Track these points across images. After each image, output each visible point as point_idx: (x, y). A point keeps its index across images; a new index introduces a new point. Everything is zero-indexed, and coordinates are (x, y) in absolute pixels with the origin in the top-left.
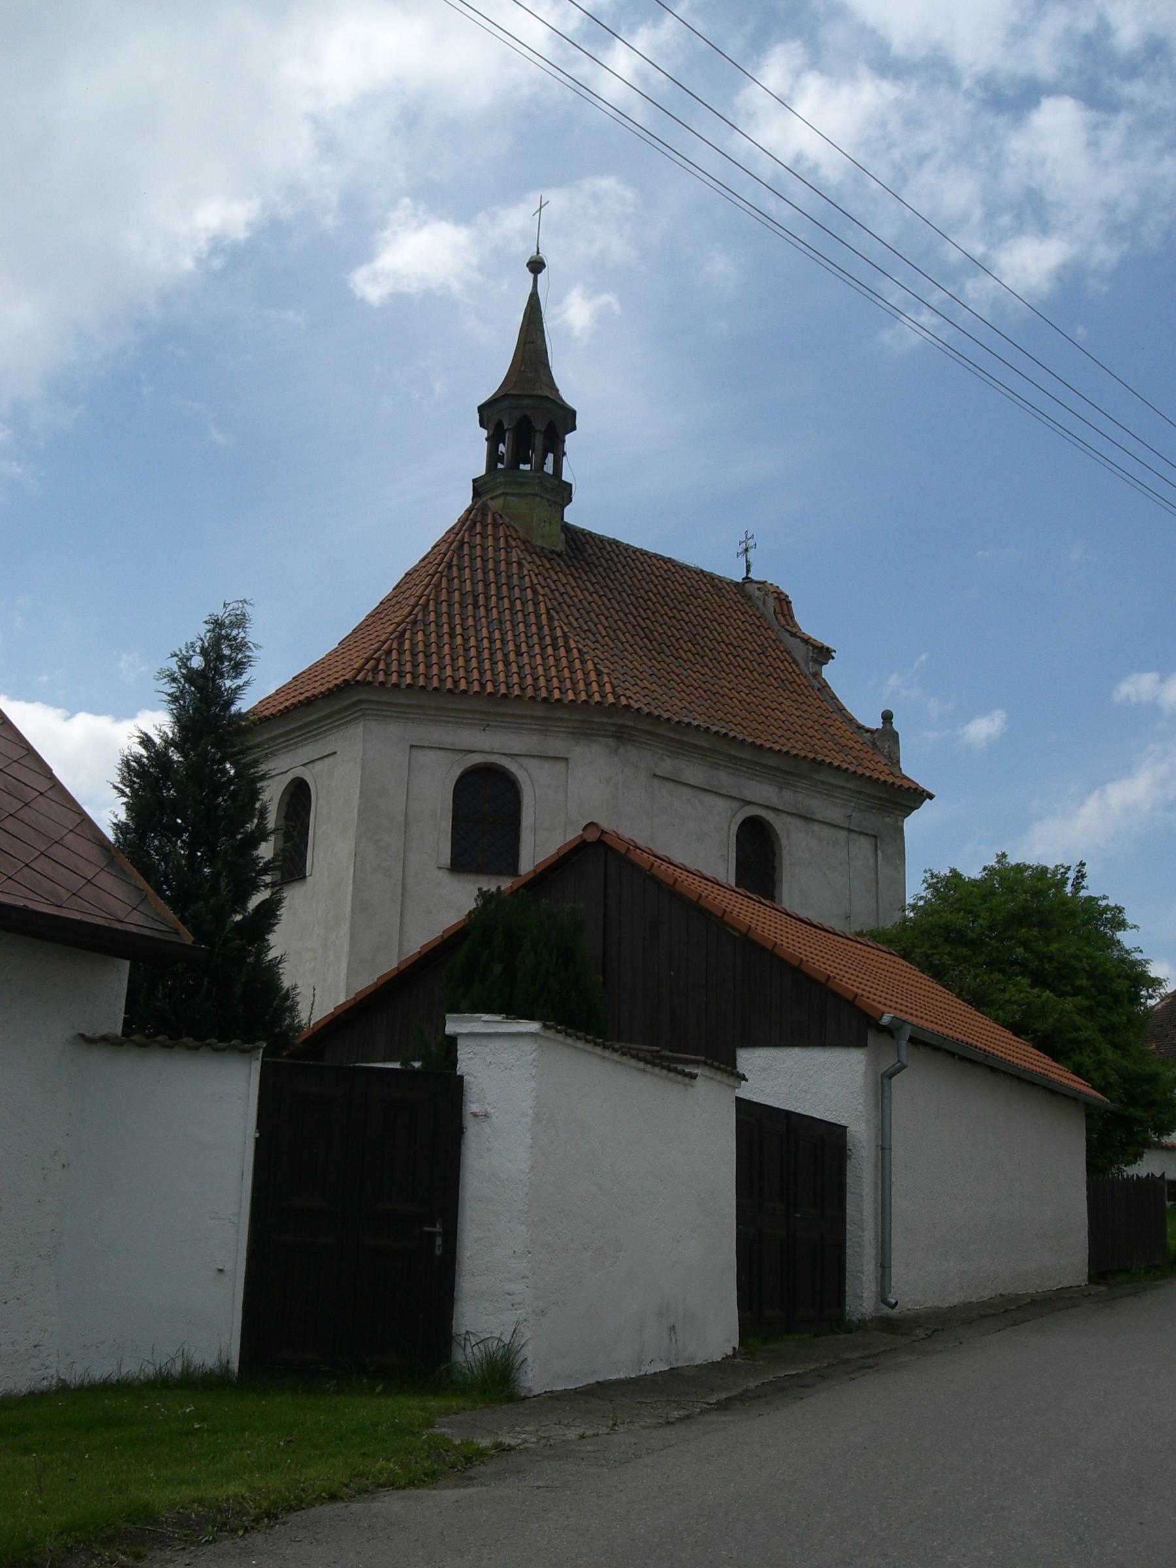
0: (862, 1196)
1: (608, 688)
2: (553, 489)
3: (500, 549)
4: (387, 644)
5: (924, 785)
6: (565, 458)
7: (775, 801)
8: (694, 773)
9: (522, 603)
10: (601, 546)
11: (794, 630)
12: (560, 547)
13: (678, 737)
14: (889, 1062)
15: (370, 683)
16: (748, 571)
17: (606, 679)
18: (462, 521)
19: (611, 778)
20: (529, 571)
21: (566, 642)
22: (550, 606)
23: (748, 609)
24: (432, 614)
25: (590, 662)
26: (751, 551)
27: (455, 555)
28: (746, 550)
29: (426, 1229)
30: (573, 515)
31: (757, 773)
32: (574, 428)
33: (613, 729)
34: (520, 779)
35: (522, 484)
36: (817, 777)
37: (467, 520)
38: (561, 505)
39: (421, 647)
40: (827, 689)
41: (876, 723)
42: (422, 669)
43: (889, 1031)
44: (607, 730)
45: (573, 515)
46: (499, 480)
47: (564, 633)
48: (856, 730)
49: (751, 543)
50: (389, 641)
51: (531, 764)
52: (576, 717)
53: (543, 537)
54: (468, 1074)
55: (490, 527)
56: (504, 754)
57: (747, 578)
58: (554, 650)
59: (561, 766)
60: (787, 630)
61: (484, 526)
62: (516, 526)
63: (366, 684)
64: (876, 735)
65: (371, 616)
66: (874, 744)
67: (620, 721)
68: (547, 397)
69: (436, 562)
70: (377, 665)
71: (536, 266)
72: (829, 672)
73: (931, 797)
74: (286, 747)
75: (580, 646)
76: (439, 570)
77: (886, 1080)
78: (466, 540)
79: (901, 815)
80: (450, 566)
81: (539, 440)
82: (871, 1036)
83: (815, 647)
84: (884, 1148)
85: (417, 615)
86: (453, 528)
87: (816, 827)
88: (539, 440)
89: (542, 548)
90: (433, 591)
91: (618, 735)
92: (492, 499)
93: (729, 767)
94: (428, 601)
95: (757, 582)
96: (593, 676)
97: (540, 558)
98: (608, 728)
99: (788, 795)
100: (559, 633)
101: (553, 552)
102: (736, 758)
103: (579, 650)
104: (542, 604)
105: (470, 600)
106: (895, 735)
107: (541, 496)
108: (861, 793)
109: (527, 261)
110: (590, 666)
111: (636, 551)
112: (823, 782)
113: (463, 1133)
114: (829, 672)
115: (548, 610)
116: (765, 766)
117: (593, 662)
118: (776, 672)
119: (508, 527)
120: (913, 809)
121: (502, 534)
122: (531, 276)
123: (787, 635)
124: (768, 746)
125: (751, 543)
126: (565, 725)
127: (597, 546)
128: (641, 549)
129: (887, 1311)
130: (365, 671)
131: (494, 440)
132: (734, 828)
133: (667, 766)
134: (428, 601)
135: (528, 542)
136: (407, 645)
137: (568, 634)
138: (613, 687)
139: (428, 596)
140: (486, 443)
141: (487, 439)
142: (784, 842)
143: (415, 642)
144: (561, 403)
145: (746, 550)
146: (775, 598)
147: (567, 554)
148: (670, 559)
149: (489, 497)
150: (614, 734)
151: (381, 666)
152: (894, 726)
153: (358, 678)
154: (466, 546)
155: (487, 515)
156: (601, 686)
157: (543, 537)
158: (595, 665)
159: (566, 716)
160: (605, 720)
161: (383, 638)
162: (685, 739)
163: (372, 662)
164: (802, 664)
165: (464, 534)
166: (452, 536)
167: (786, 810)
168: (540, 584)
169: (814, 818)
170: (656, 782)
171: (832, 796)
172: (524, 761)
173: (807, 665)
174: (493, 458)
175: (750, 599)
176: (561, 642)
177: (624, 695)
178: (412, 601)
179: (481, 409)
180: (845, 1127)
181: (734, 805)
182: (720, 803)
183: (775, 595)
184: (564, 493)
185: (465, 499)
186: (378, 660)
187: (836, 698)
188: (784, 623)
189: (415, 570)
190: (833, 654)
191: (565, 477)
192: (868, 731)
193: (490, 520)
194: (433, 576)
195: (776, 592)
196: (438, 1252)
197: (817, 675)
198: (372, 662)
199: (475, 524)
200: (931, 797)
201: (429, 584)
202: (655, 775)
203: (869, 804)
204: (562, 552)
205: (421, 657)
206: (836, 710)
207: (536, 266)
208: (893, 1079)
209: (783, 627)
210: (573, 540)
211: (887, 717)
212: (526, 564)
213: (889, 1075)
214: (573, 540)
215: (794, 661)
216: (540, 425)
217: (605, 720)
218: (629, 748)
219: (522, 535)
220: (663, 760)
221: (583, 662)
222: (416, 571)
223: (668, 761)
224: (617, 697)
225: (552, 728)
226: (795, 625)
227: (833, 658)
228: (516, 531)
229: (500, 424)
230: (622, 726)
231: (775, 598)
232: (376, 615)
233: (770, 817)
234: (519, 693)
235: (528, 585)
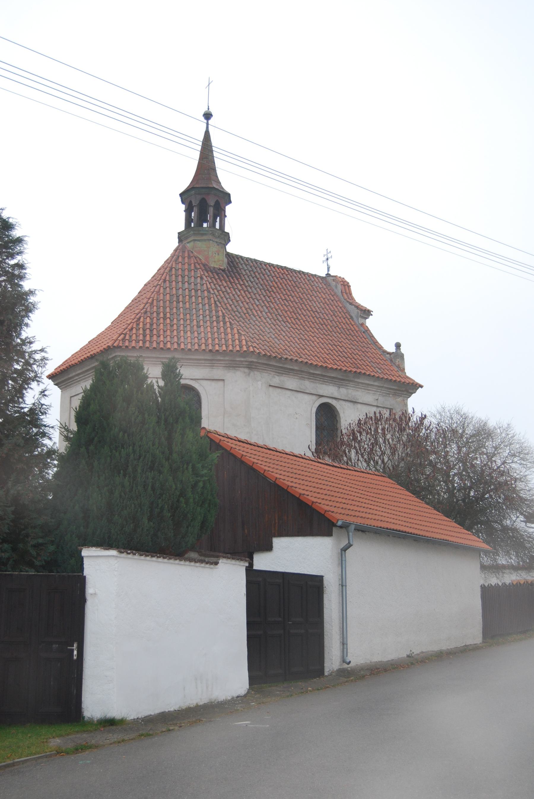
0: (331, 610)
1: (244, 342)
2: (219, 236)
3: (191, 270)
4: (130, 325)
5: (418, 380)
6: (226, 219)
7: (336, 395)
8: (291, 382)
9: (202, 298)
10: (247, 263)
11: (351, 301)
12: (224, 266)
13: (281, 365)
14: (344, 543)
15: (121, 347)
16: (328, 270)
17: (243, 338)
18: (172, 256)
19: (247, 389)
20: (206, 281)
21: (224, 319)
22: (216, 299)
23: (328, 291)
24: (155, 307)
25: (235, 329)
26: (329, 260)
27: (168, 275)
28: (327, 259)
29: (69, 648)
30: (231, 248)
31: (326, 381)
32: (179, 233)
33: (247, 363)
34: (200, 391)
35: (203, 235)
36: (356, 380)
37: (174, 255)
38: (224, 244)
39: (148, 326)
40: (368, 332)
41: (391, 348)
42: (148, 338)
43: (345, 527)
44: (243, 364)
45: (231, 248)
46: (191, 233)
47: (223, 314)
48: (382, 353)
49: (329, 255)
50: (132, 324)
51: (205, 383)
52: (227, 358)
53: (215, 262)
54: (88, 575)
55: (186, 258)
56: (191, 379)
57: (328, 275)
58: (217, 323)
59: (221, 383)
60: (348, 301)
61: (184, 258)
62: (200, 257)
63: (119, 347)
64: (392, 356)
65: (127, 308)
66: (391, 361)
67: (250, 360)
68: (214, 188)
69: (158, 279)
70: (125, 337)
71: (208, 116)
72: (370, 323)
73: (421, 387)
74: (83, 379)
75: (231, 320)
76: (159, 284)
77: (343, 552)
78: (173, 266)
79: (405, 397)
80: (165, 281)
81: (211, 210)
82: (334, 529)
83: (361, 310)
84: (343, 585)
85: (147, 309)
86: (168, 260)
87: (359, 406)
88: (211, 210)
89: (214, 268)
90: (156, 295)
91: (250, 366)
92: (188, 243)
93: (310, 379)
94: (153, 300)
95: (333, 276)
96: (237, 336)
97: (212, 273)
98: (244, 363)
99: (343, 391)
100: (220, 313)
101: (220, 269)
102: (314, 374)
103: (230, 322)
104: (212, 299)
105: (175, 299)
106: (402, 356)
107: (212, 240)
108: (382, 387)
109: (203, 114)
110: (236, 331)
111: (266, 264)
112: (362, 383)
113: (86, 602)
114: (370, 323)
115: (215, 302)
116: (330, 377)
117: (237, 329)
118: (341, 325)
119: (196, 258)
120: (412, 393)
121: (192, 262)
122: (206, 121)
123: (348, 304)
124: (330, 367)
125: (329, 255)
126: (222, 363)
127: (245, 264)
128: (270, 263)
129: (345, 666)
130: (118, 341)
131: (188, 211)
132: (314, 410)
133: (276, 380)
134: (153, 300)
135: (207, 265)
136: (141, 325)
137: (225, 314)
138: (246, 342)
139: (153, 298)
140: (184, 213)
141: (185, 211)
142: (341, 415)
143: (145, 323)
144: (221, 190)
145: (327, 259)
146: (341, 285)
147: (228, 270)
148: (285, 267)
149: (186, 242)
150: (248, 366)
151: (127, 337)
152: (401, 350)
153: (114, 345)
154: (173, 269)
155: (185, 252)
156: (240, 341)
157: (215, 262)
158: (238, 330)
159: (222, 358)
160: (242, 359)
161: (128, 322)
162: (285, 366)
163: (122, 336)
164: (355, 319)
165: (173, 263)
166: (167, 264)
167: (342, 398)
168: (211, 288)
169: (357, 401)
170: (271, 389)
171: (368, 390)
172: (202, 382)
173: (358, 319)
174: (188, 220)
175: (329, 285)
176: (221, 319)
177: (252, 346)
178: (145, 301)
179: (181, 195)
180: (322, 577)
181: (314, 397)
182: (306, 397)
183: (342, 283)
184: (226, 238)
185: (175, 243)
186: (125, 334)
187: (373, 336)
188: (346, 297)
189: (149, 283)
190: (372, 313)
191: (226, 230)
192: (388, 353)
193: (186, 255)
194: (156, 287)
195: (342, 281)
196: (75, 658)
197: (363, 325)
198: (122, 336)
199: (178, 257)
200: (421, 387)
201: (154, 291)
202: (270, 386)
203: (388, 392)
204: (225, 269)
205: (148, 332)
206: (373, 343)
207: (208, 116)
208: (346, 551)
209: (346, 299)
210: (232, 262)
211: (398, 346)
212: (205, 277)
213: (344, 550)
214: (232, 262)
215: (351, 317)
216: (211, 202)
217: (242, 359)
218: (256, 372)
219: (203, 261)
220: (275, 377)
221: (232, 329)
222: (149, 283)
223: (277, 378)
224: (248, 347)
225: (216, 365)
226: (353, 298)
227: (372, 315)
228: (200, 260)
229: (191, 202)
230: (251, 362)
231: (341, 285)
232: (129, 308)
233: (333, 402)
234: (197, 348)
235: (205, 288)
